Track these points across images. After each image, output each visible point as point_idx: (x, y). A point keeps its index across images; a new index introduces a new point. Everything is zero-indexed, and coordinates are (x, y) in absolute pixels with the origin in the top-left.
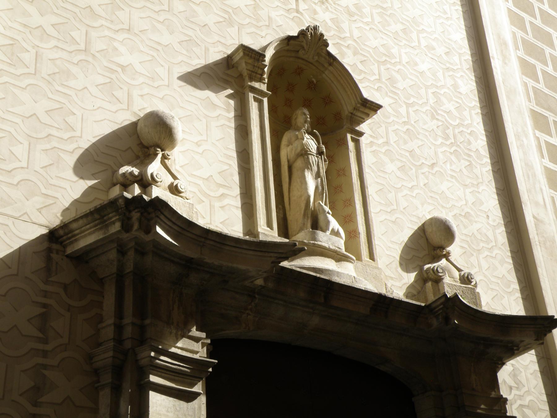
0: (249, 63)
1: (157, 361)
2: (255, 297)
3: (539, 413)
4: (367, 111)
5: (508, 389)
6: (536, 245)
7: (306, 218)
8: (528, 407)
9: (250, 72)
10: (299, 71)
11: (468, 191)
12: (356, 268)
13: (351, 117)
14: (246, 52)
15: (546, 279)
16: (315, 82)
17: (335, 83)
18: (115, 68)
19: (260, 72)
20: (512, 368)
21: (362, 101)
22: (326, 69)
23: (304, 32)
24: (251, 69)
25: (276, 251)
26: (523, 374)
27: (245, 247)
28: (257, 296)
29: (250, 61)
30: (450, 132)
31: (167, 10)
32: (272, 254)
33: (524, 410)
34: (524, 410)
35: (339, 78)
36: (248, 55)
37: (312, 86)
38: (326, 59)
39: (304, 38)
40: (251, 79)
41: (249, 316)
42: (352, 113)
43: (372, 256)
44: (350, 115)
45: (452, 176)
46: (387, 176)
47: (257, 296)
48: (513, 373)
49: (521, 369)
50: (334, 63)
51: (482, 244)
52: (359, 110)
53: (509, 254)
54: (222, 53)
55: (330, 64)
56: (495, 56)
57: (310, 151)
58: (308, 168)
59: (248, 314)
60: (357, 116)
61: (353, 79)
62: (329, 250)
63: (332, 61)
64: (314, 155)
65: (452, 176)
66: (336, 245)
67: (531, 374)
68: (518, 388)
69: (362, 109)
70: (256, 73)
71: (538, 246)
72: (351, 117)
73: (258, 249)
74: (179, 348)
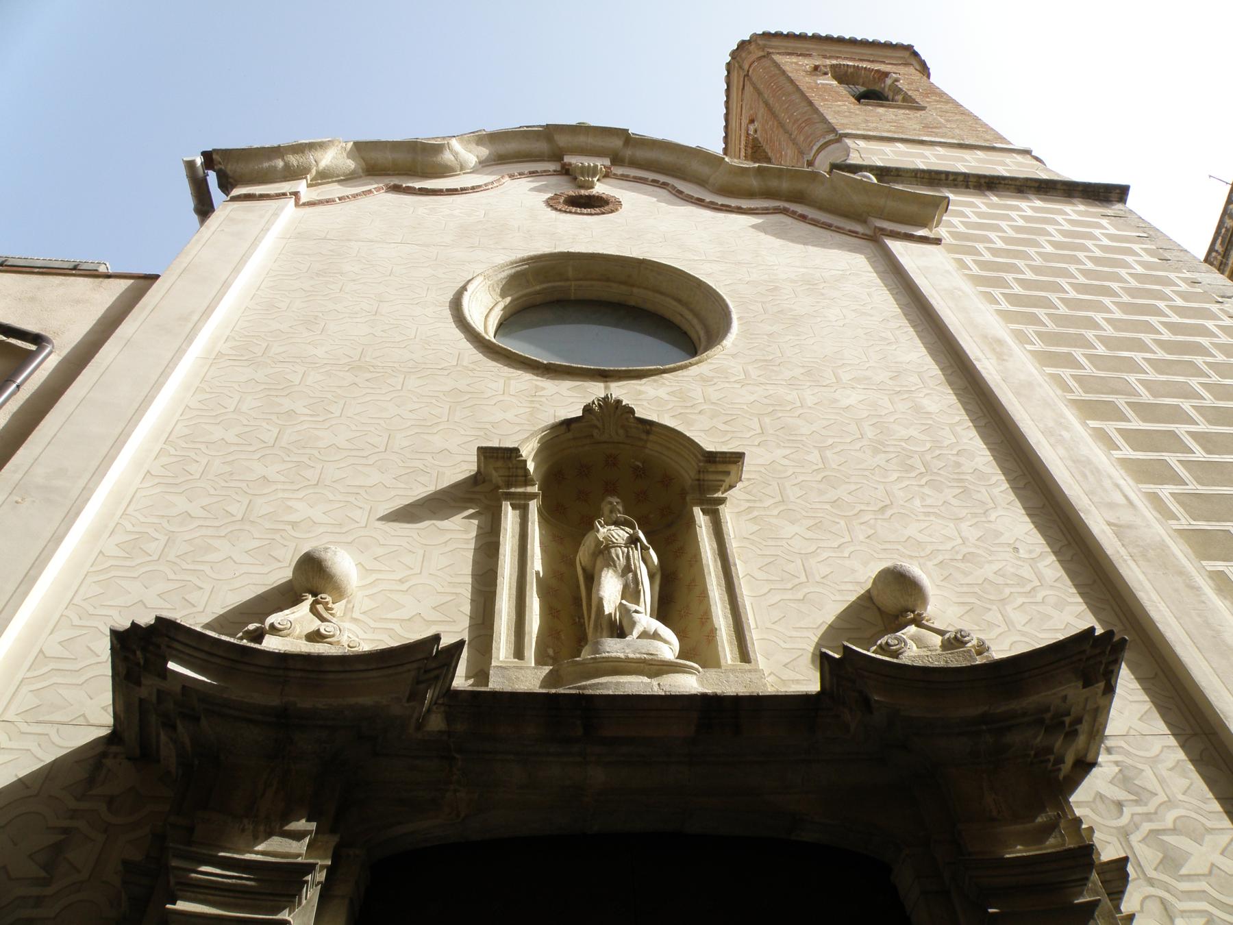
1: (193, 875)
3: (1208, 838)
4: (721, 468)
5: (1113, 808)
6: (1125, 561)
8: (1174, 830)
11: (964, 526)
15: (1162, 606)
18: (281, 527)
19: (521, 472)
20: (1117, 769)
26: (1148, 772)
27: (361, 667)
28: (458, 756)
29: (500, 464)
30: (916, 461)
32: (408, 666)
33: (1165, 838)
34: (1165, 838)
36: (492, 457)
37: (639, 473)
40: (509, 485)
45: (927, 514)
46: (784, 543)
47: (458, 756)
48: (1120, 776)
49: (1140, 766)
51: (1007, 591)
53: (1074, 590)
55: (648, 433)
56: (980, 355)
58: (608, 566)
65: (927, 514)
67: (1171, 769)
68: (1137, 802)
69: (712, 468)
71: (1130, 562)
74: (257, 853)
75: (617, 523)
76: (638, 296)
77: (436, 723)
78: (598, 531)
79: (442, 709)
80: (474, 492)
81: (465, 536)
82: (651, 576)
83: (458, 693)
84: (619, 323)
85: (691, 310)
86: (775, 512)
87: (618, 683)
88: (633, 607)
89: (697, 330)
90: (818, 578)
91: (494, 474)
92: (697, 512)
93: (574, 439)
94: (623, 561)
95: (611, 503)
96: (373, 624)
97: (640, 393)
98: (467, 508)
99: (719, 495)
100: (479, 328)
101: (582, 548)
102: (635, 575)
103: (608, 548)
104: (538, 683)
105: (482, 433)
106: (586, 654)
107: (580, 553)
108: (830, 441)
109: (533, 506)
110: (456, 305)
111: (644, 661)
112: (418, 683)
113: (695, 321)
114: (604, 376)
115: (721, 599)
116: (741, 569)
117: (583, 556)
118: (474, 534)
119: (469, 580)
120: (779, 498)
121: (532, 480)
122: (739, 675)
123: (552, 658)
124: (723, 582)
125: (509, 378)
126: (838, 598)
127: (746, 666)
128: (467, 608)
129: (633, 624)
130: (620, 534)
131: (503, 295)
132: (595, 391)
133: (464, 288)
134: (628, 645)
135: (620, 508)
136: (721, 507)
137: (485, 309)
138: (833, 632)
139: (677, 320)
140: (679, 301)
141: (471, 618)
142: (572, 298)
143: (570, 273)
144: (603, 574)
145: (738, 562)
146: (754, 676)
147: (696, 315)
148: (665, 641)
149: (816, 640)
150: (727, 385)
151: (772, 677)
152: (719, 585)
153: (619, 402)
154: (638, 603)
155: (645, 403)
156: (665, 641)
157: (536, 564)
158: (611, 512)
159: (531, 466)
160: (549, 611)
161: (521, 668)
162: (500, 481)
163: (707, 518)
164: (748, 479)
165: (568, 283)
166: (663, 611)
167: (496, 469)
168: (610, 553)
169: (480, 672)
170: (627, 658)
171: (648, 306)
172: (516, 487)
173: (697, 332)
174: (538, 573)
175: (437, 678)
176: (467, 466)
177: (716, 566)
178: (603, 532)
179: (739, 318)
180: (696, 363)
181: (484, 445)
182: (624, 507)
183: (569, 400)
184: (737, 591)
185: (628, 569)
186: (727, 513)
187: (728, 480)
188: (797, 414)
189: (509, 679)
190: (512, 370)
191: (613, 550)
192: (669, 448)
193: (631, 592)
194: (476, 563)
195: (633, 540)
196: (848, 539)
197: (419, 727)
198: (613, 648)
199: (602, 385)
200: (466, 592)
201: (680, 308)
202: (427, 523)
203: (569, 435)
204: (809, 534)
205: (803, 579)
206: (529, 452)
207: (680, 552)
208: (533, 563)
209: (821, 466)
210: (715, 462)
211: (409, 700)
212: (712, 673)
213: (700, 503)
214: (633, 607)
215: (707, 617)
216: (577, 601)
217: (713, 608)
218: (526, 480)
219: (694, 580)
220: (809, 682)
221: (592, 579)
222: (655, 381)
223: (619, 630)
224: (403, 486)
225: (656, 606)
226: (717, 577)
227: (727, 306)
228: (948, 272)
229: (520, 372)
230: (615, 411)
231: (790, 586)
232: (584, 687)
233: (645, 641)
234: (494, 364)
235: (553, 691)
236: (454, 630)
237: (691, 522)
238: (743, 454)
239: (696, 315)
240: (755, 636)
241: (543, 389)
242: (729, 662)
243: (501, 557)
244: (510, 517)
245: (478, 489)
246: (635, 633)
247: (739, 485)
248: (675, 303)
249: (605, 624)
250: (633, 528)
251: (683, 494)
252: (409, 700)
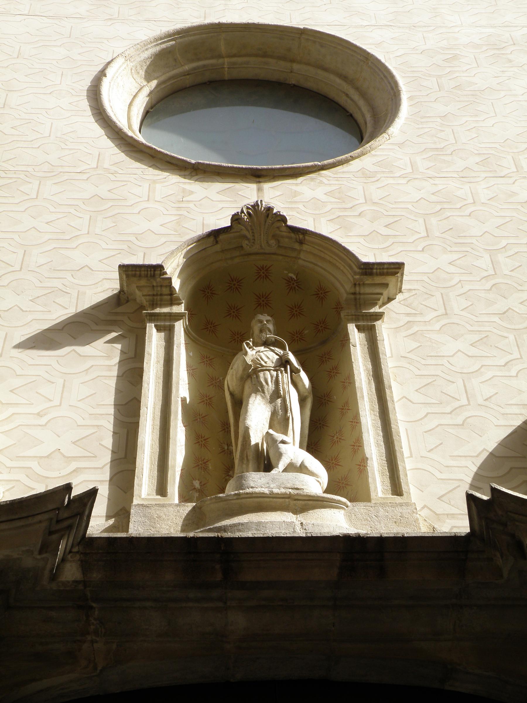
0: (143, 286)
2: (92, 608)
4: (378, 280)
7: (245, 462)
9: (151, 298)
10: (264, 273)
12: (349, 517)
13: (355, 299)
14: (130, 273)
16: (294, 277)
17: (320, 264)
19: (166, 291)
21: (360, 268)
22: (299, 251)
23: (236, 217)
24: (151, 293)
25: (44, 510)
28: (94, 605)
29: (143, 282)
31: (519, 357)
32: (39, 518)
35: (322, 255)
36: (135, 276)
37: (295, 284)
38: (290, 238)
39: (239, 223)
40: (154, 305)
41: (95, 645)
42: (354, 294)
43: (396, 488)
44: (352, 296)
47: (94, 605)
50: (307, 237)
52: (364, 284)
54: (110, 290)
55: (301, 242)
57: (263, 366)
58: (256, 391)
59: (92, 642)
60: (364, 294)
61: (340, 245)
62: (272, 496)
63: (301, 236)
64: (269, 370)
66: (289, 485)
69: (369, 280)
70: (161, 295)
72: (355, 299)
73: (17, 517)
75: (266, 344)
76: (301, 74)
77: (71, 572)
78: (246, 353)
79: (78, 557)
80: (117, 314)
81: (108, 363)
82: (302, 401)
83: (93, 540)
84: (278, 104)
85: (357, 89)
86: (437, 327)
87: (259, 524)
88: (280, 437)
89: (364, 114)
90: (480, 401)
91: (138, 293)
92: (352, 328)
93: (223, 251)
94: (272, 386)
95: (261, 322)
96: (9, 464)
97: (296, 194)
98: (109, 332)
99: (376, 309)
100: (122, 122)
101: (230, 372)
102: (284, 401)
103: (256, 372)
104: (180, 522)
105: (125, 247)
106: (230, 490)
107: (228, 377)
108: (504, 243)
109: (180, 327)
110: (95, 94)
111: (289, 496)
112: (51, 533)
113: (361, 103)
114: (257, 176)
115: (374, 426)
116: (396, 392)
117: (231, 380)
118: (117, 359)
119: (111, 410)
120: (442, 311)
121: (178, 299)
122: (389, 509)
124: (377, 407)
125: (155, 182)
126: (502, 422)
127: (398, 499)
128: (108, 441)
129: (280, 455)
130: (269, 356)
131: (148, 78)
132: (246, 195)
133: (102, 73)
134: (273, 480)
135: (271, 326)
136: (378, 324)
137: (128, 97)
138: (479, 478)
139: (342, 100)
140: (344, 78)
141: (113, 452)
142: (226, 77)
143: (223, 48)
145: (394, 384)
146: (405, 510)
147: (363, 95)
148: (311, 474)
149: (475, 469)
150: (391, 181)
151: (426, 511)
153: (269, 209)
154: (285, 433)
155: (300, 206)
156: (311, 474)
157: (182, 389)
158: (261, 331)
159: (176, 284)
160: (197, 440)
161: (163, 506)
162: (144, 301)
163: (362, 335)
164: (410, 290)
165: (221, 61)
166: (313, 444)
167: (139, 288)
168: (258, 377)
169: (121, 512)
170: (272, 493)
171: (310, 85)
172: (161, 306)
173: (363, 116)
174: (184, 400)
175: (70, 528)
176: (109, 285)
178: (251, 354)
179: (410, 98)
180: (358, 157)
181: (127, 262)
182: (276, 324)
183: (217, 205)
184: (391, 416)
185: (276, 394)
186: (383, 329)
187: (386, 293)
188: (467, 212)
189: (151, 518)
190: (157, 172)
191: (261, 374)
192: (323, 259)
193: (280, 420)
194: (118, 391)
195: (283, 363)
196: (516, 355)
197: (53, 577)
198: (258, 482)
199: (253, 186)
200: (108, 424)
201: (345, 87)
202: (67, 349)
203: (218, 247)
204: (473, 351)
205: (464, 401)
206: (174, 269)
207: (334, 371)
209: (492, 272)
210: (371, 274)
211: (40, 552)
212: (360, 508)
213: (356, 318)
214: (280, 437)
215: (358, 444)
216: (226, 426)
217: (365, 436)
218: (173, 300)
219: (347, 403)
220: (459, 524)
221: (239, 404)
222: (312, 179)
223: (265, 463)
224: (41, 309)
225: (307, 431)
226: (371, 401)
227: (396, 83)
229: (166, 174)
230: (262, 221)
231: (448, 409)
232: (224, 529)
234: (138, 165)
236: (91, 474)
237: (345, 340)
238: (403, 264)
239: (363, 95)
240: (408, 465)
241: (191, 193)
243: (145, 385)
244: (154, 340)
245: (120, 309)
246: (282, 465)
247: (399, 297)
248: (338, 80)
249: (251, 455)
251: (338, 308)
252: (40, 552)
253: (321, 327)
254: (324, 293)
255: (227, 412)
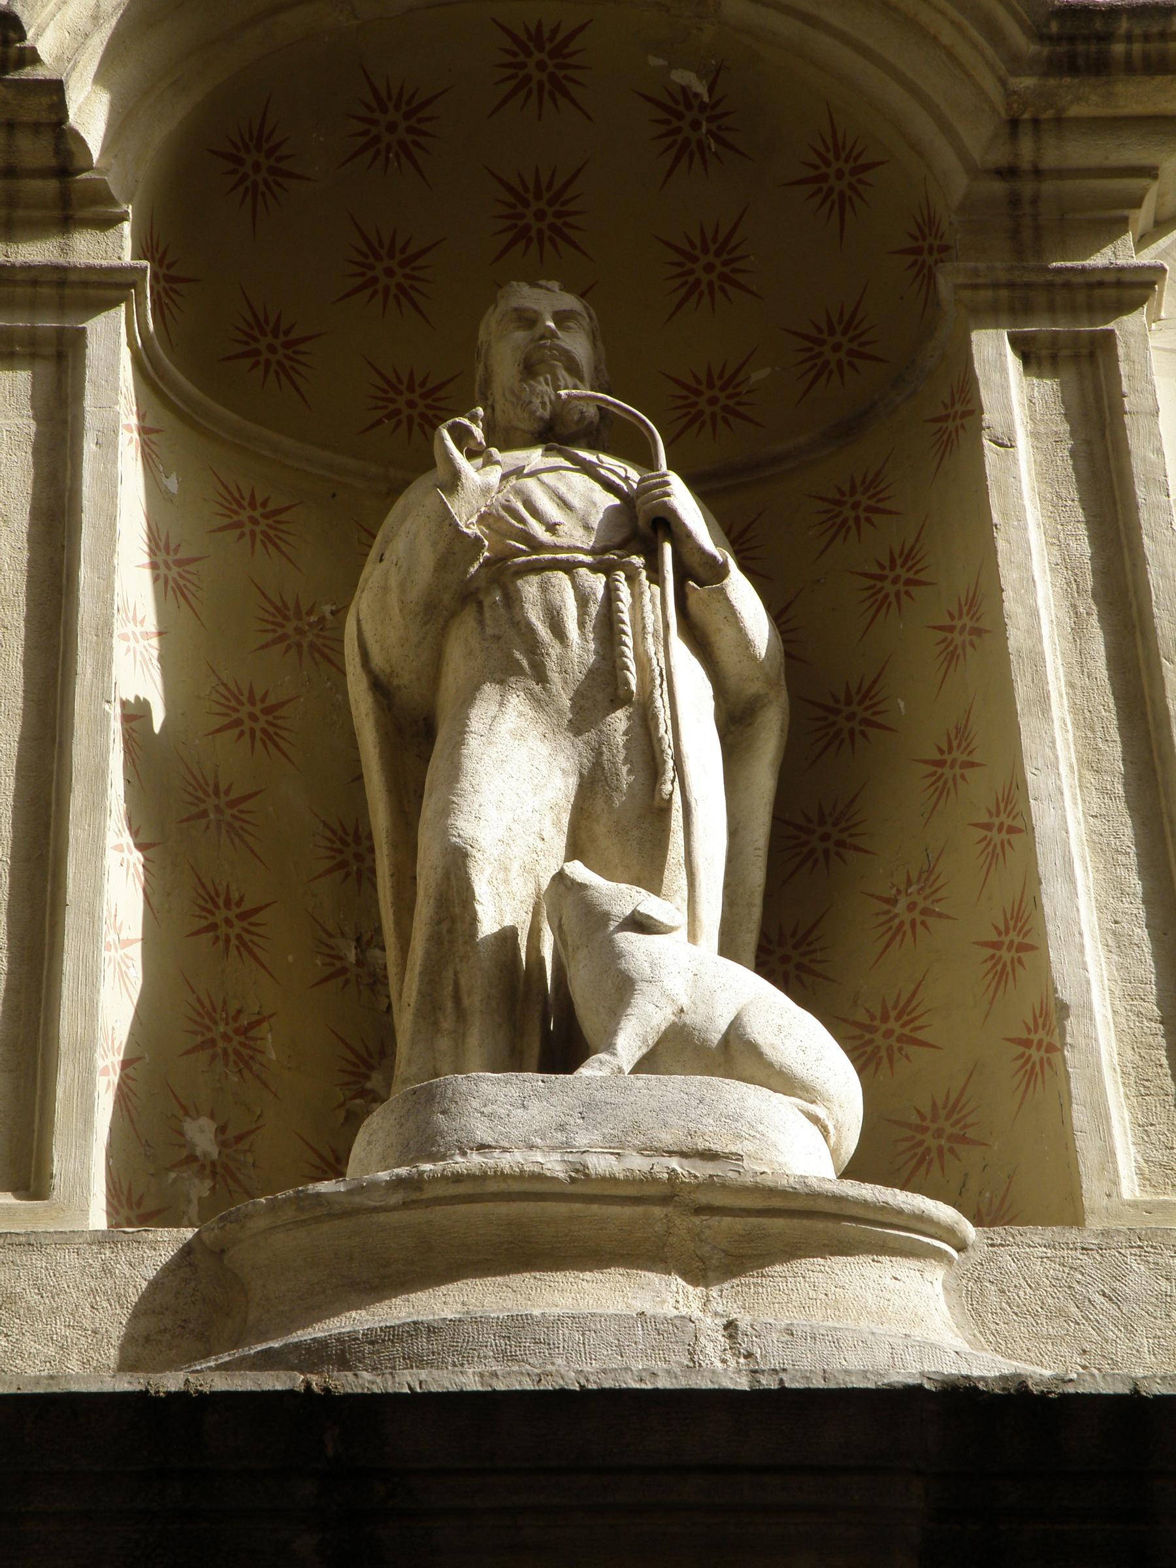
12: (971, 1301)
16: (700, 88)
19: (34, 151)
21: (1042, 37)
42: (1009, 172)
44: (999, 187)
57: (536, 546)
58: (503, 673)
60: (1061, 173)
62: (583, 1188)
66: (667, 1138)
69: (1085, 100)
72: (1014, 201)
75: (556, 434)
78: (453, 481)
82: (734, 723)
87: (517, 1325)
88: (621, 897)
92: (994, 355)
94: (580, 647)
95: (529, 320)
99: (1122, 253)
101: (372, 574)
102: (645, 719)
104: (114, 1323)
107: (364, 604)
109: (111, 349)
111: (669, 1193)
115: (1098, 845)
117: (377, 616)
121: (101, 195)
123: (213, 1170)
124: (1114, 751)
129: (622, 988)
130: (570, 497)
134: (589, 1110)
135: (578, 344)
144: (479, 717)
148: (783, 1081)
152: (1090, 763)
154: (652, 880)
156: (783, 1081)
158: (529, 369)
159: (90, 114)
160: (197, 916)
161: (30, 1243)
166: (793, 927)
168: (512, 600)
170: (581, 1174)
174: (135, 714)
177: (1079, 660)
182: (600, 336)
185: (608, 687)
191: (530, 588)
193: (623, 815)
195: (641, 530)
207: (899, 576)
208: (104, 664)
212: (1029, 1255)
213: (1013, 302)
214: (621, 897)
215: (1017, 938)
216: (350, 850)
217: (1052, 896)
218: (71, 198)
219: (962, 732)
221: (420, 740)
223: (549, 1025)
226: (1084, 722)
228: (485, 1106)
232: (341, 1353)
233: (675, 1088)
235: (172, 1382)
242: (1130, 1188)
246: (629, 1042)
250: (643, 458)
251: (925, 247)
253: (837, 348)
254: (854, 172)
255: (359, 778)
